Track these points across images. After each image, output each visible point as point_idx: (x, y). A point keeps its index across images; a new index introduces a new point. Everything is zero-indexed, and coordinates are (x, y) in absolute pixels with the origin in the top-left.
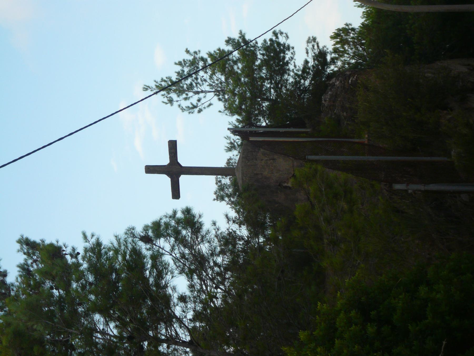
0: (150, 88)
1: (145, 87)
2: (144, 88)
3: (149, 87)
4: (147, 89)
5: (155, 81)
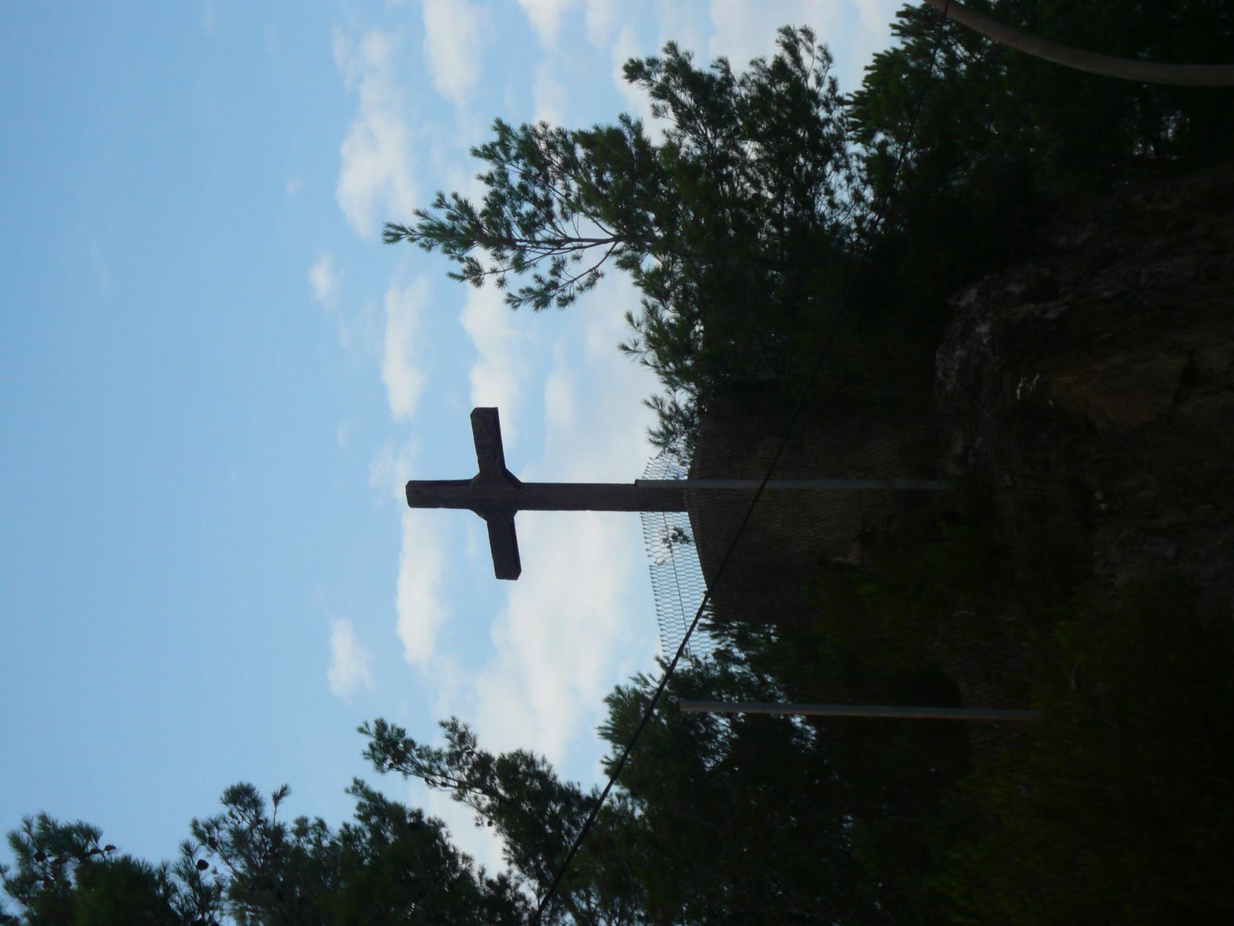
0: (407, 233)
1: (393, 231)
2: (388, 234)
3: (403, 229)
4: (397, 238)
5: (418, 213)
